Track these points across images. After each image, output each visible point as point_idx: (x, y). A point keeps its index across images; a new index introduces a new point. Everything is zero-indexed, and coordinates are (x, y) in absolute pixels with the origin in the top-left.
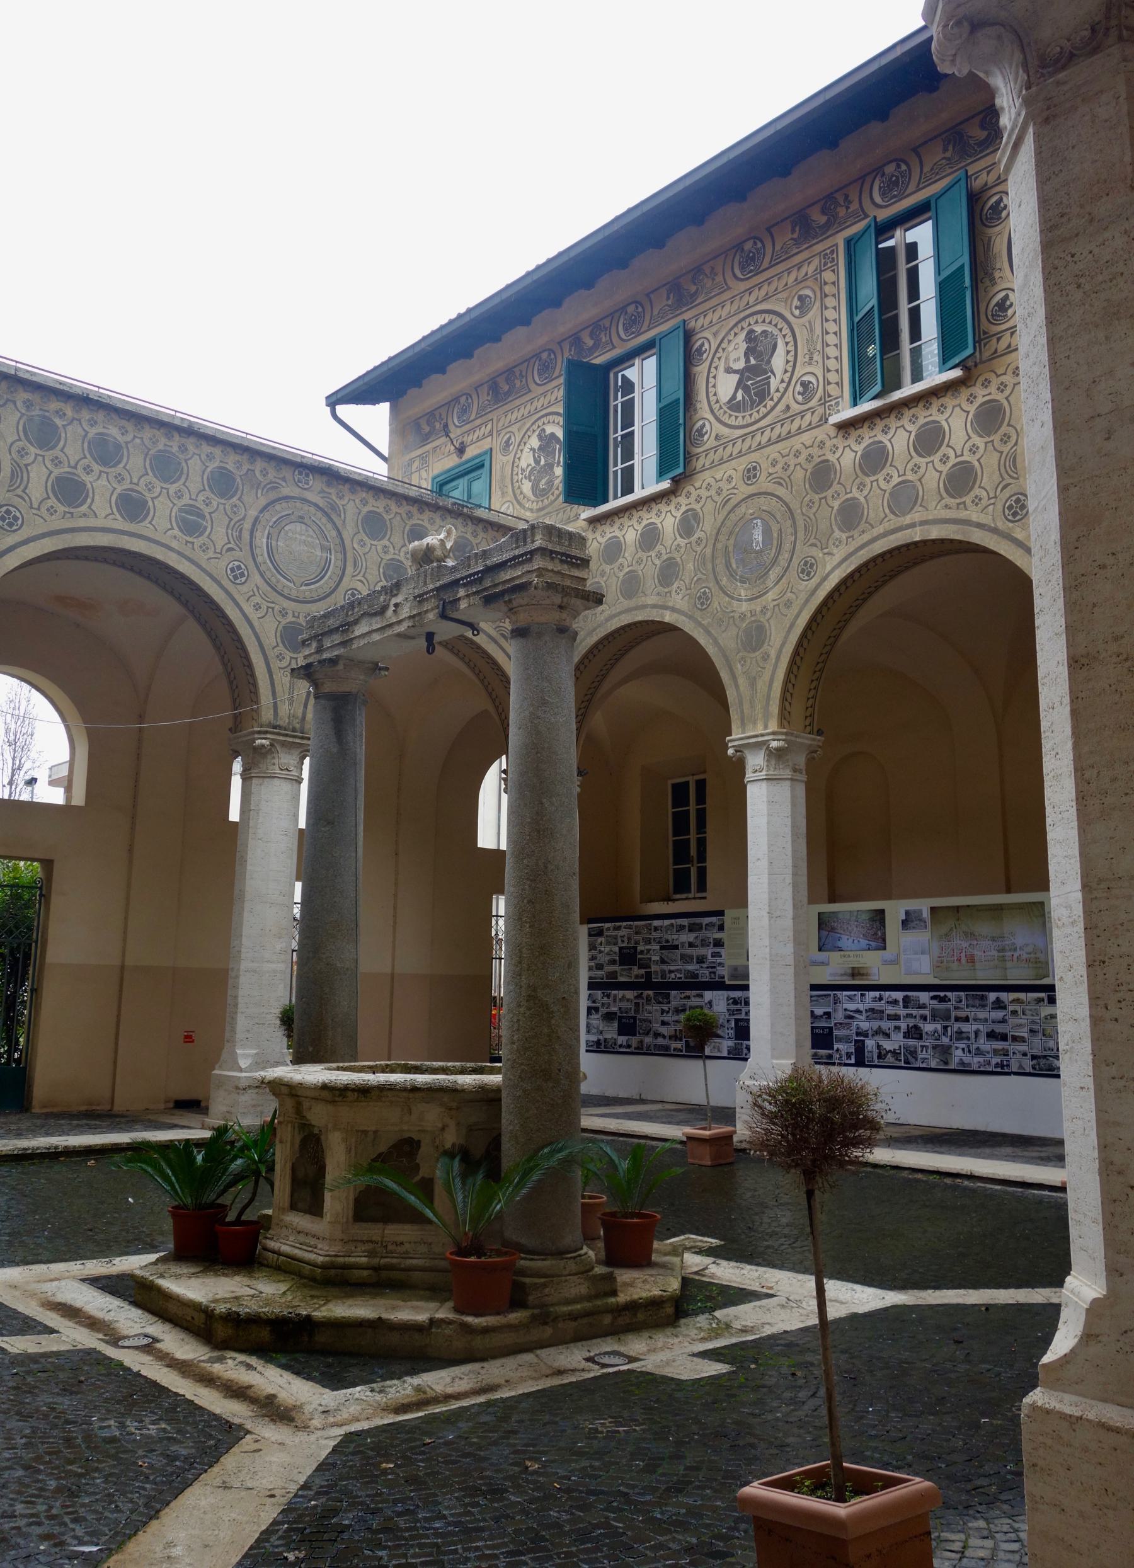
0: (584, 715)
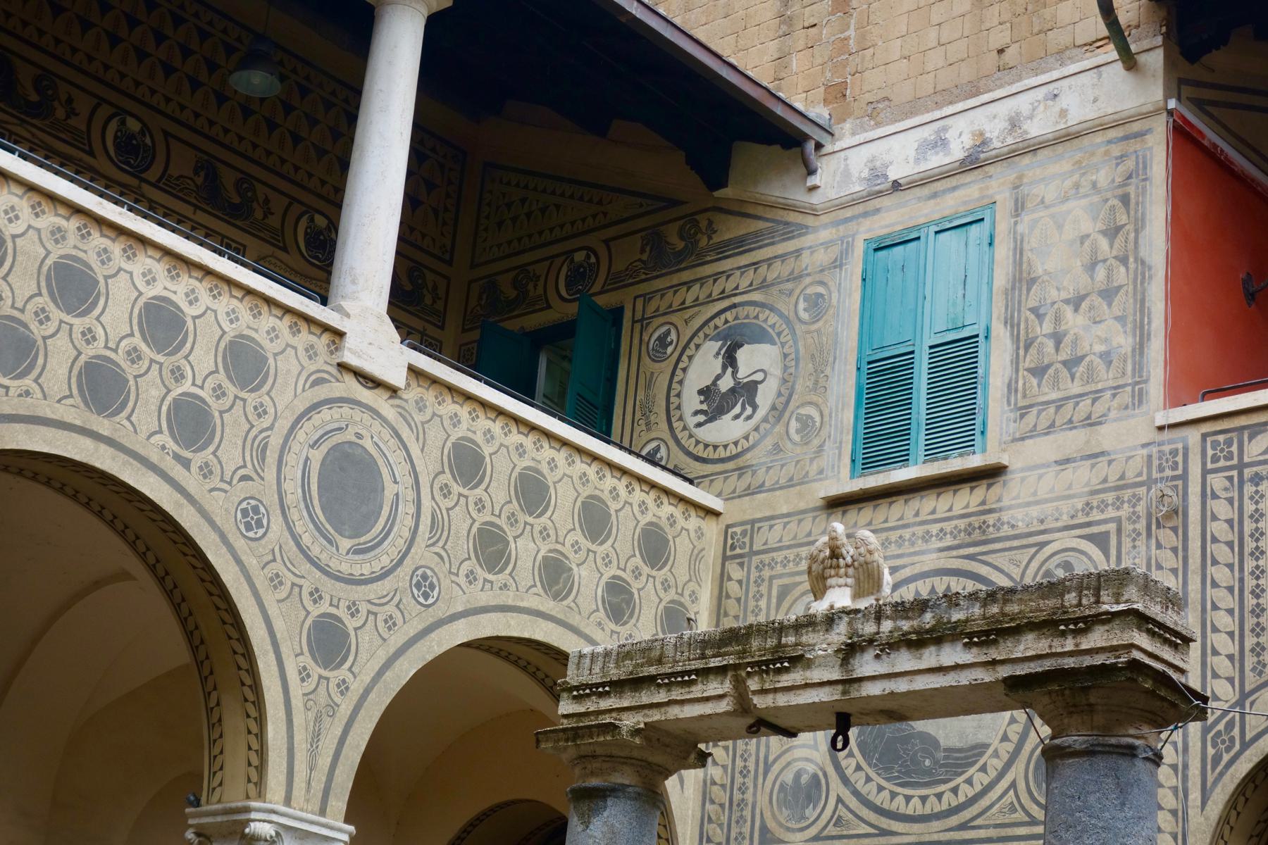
0: (488, 650)
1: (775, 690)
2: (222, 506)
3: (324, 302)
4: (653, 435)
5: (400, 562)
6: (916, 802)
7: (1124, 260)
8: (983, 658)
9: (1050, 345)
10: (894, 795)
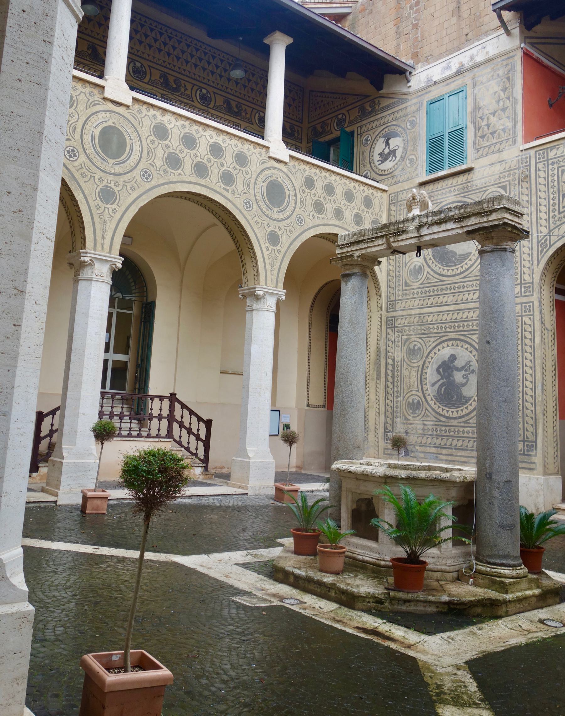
0: (318, 237)
1: (398, 241)
2: (239, 202)
3: (263, 138)
4: (366, 169)
6: (450, 271)
7: (508, 98)
8: (459, 226)
9: (486, 128)
10: (444, 270)
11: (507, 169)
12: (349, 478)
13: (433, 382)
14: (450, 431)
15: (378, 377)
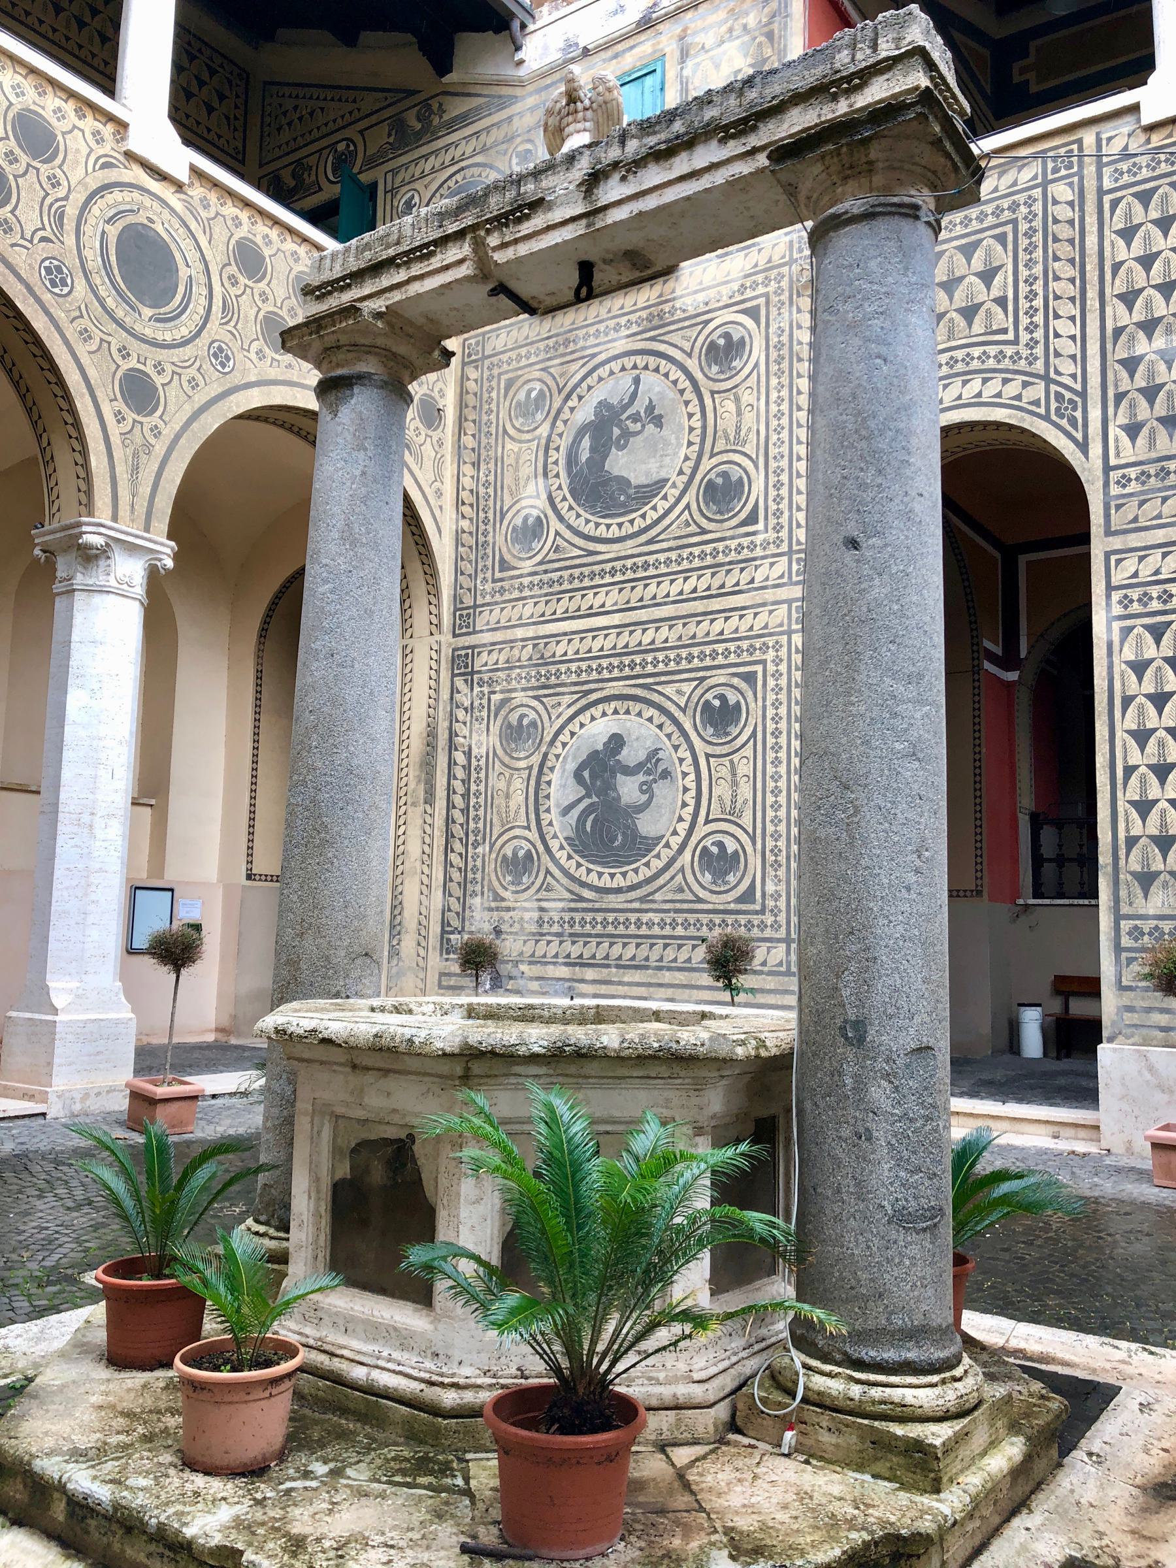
5: (198, 334)
8: (743, 149)
11: (762, 264)
12: (322, 1063)
13: (566, 803)
14: (605, 923)
15: (430, 799)
